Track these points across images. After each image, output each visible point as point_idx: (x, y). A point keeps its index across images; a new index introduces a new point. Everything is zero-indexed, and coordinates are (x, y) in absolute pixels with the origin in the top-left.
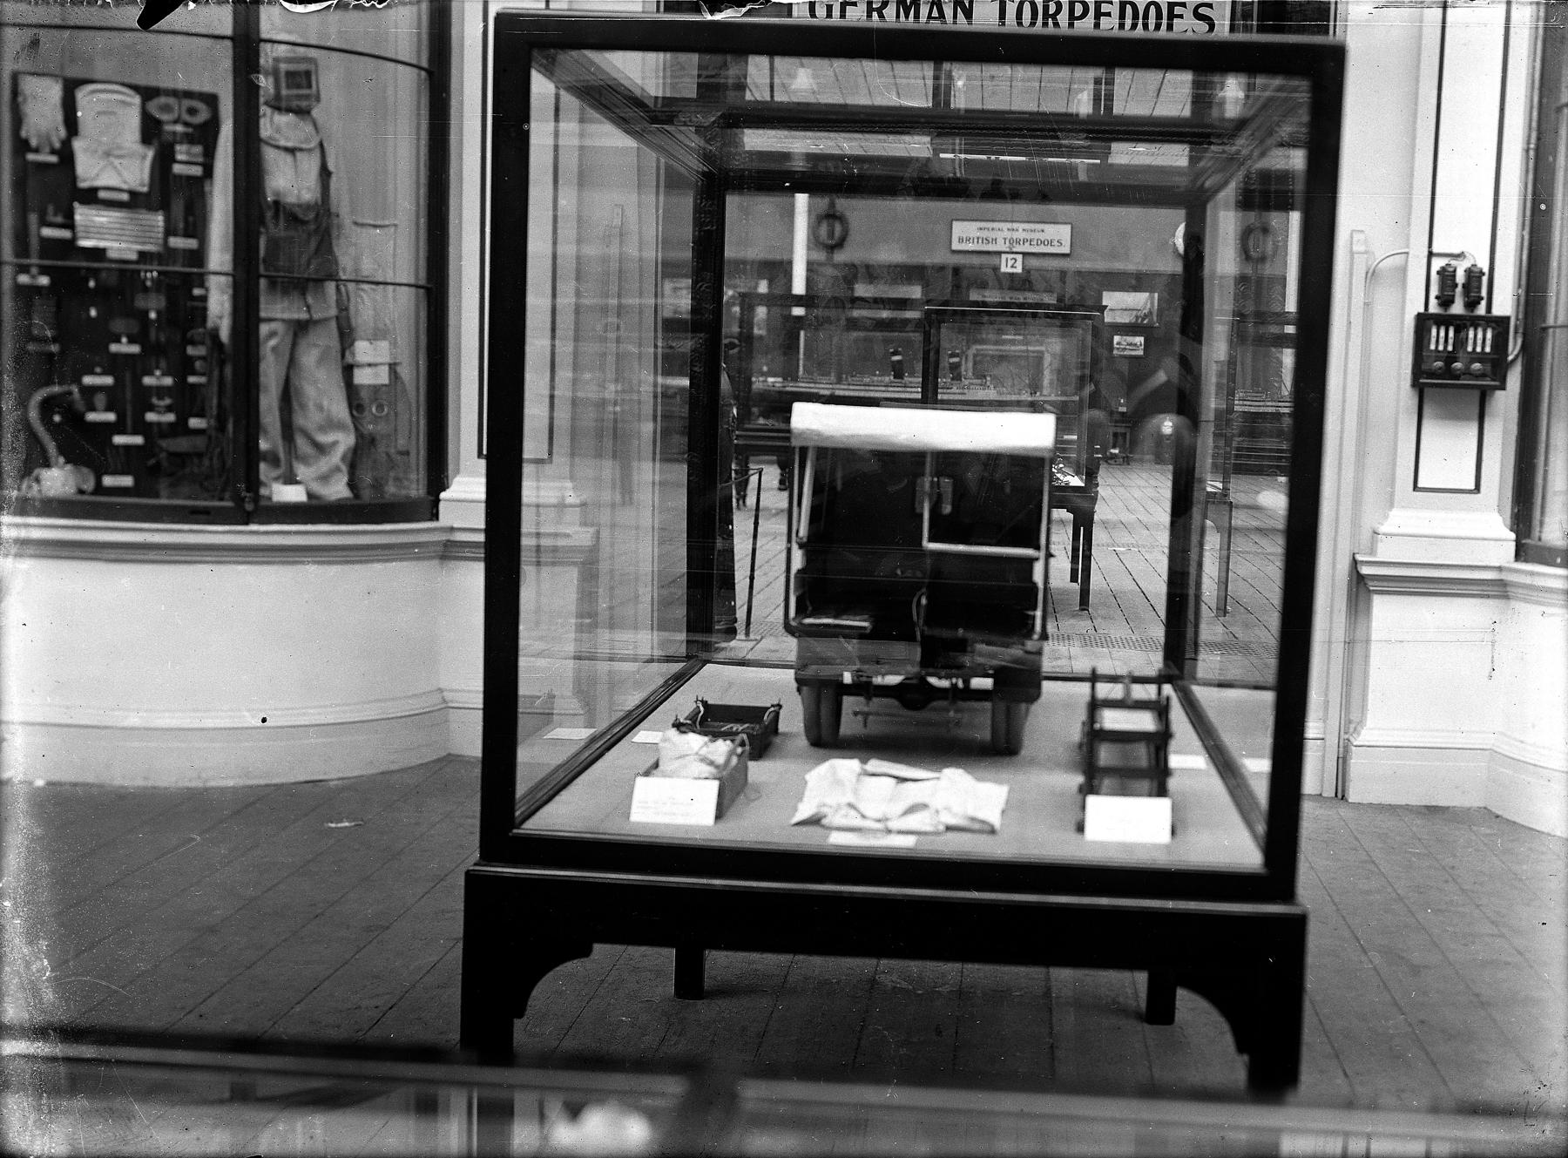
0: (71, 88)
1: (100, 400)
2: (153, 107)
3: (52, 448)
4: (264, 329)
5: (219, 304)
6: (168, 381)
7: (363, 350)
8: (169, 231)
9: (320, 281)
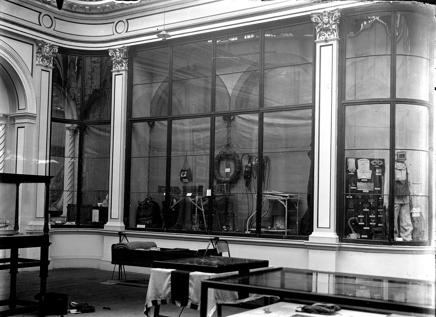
0: (357, 160)
1: (361, 220)
2: (372, 163)
3: (352, 229)
4: (395, 205)
5: (386, 202)
6: (374, 216)
7: (414, 210)
8: (375, 186)
9: (406, 196)
